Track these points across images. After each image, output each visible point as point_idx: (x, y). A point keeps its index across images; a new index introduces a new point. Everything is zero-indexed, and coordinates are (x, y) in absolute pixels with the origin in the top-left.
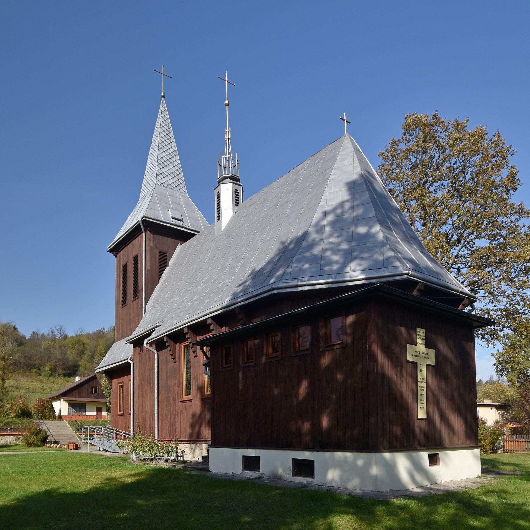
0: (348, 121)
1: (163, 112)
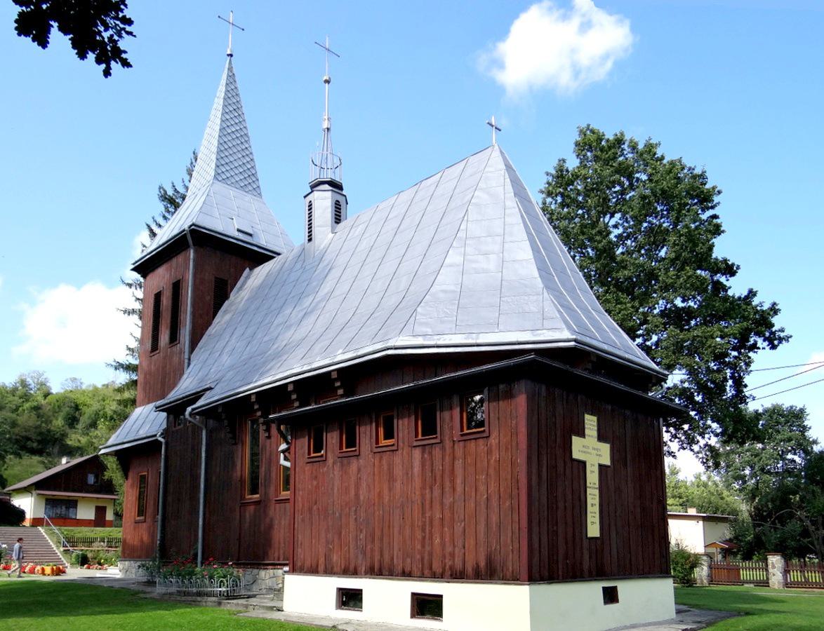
0: (498, 127)
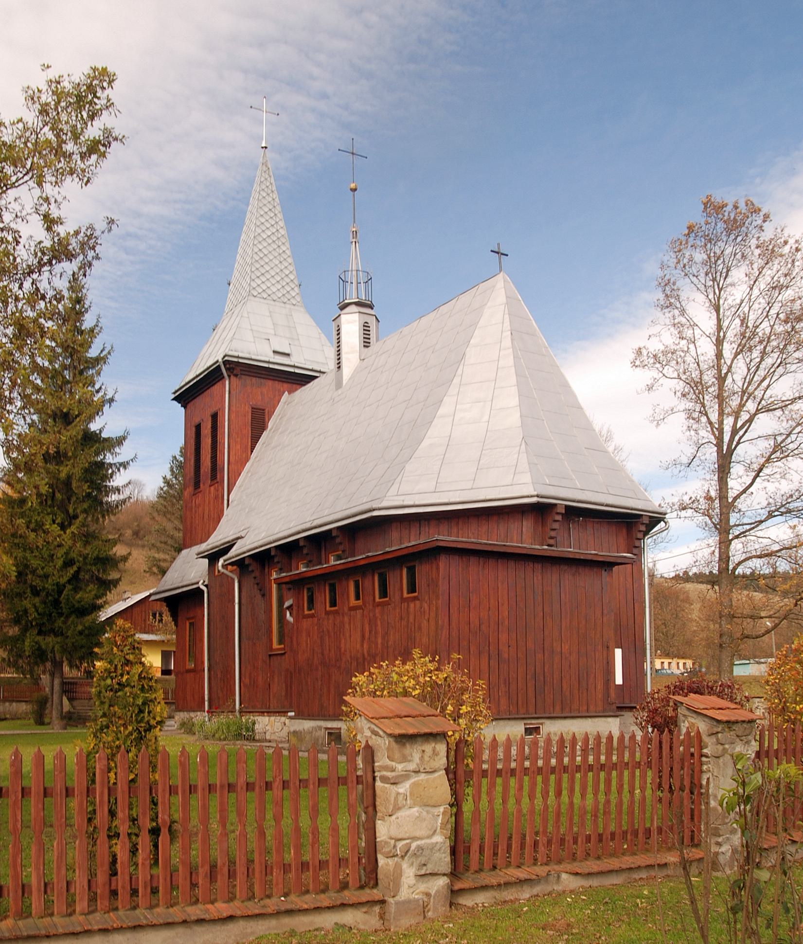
1: (263, 174)
